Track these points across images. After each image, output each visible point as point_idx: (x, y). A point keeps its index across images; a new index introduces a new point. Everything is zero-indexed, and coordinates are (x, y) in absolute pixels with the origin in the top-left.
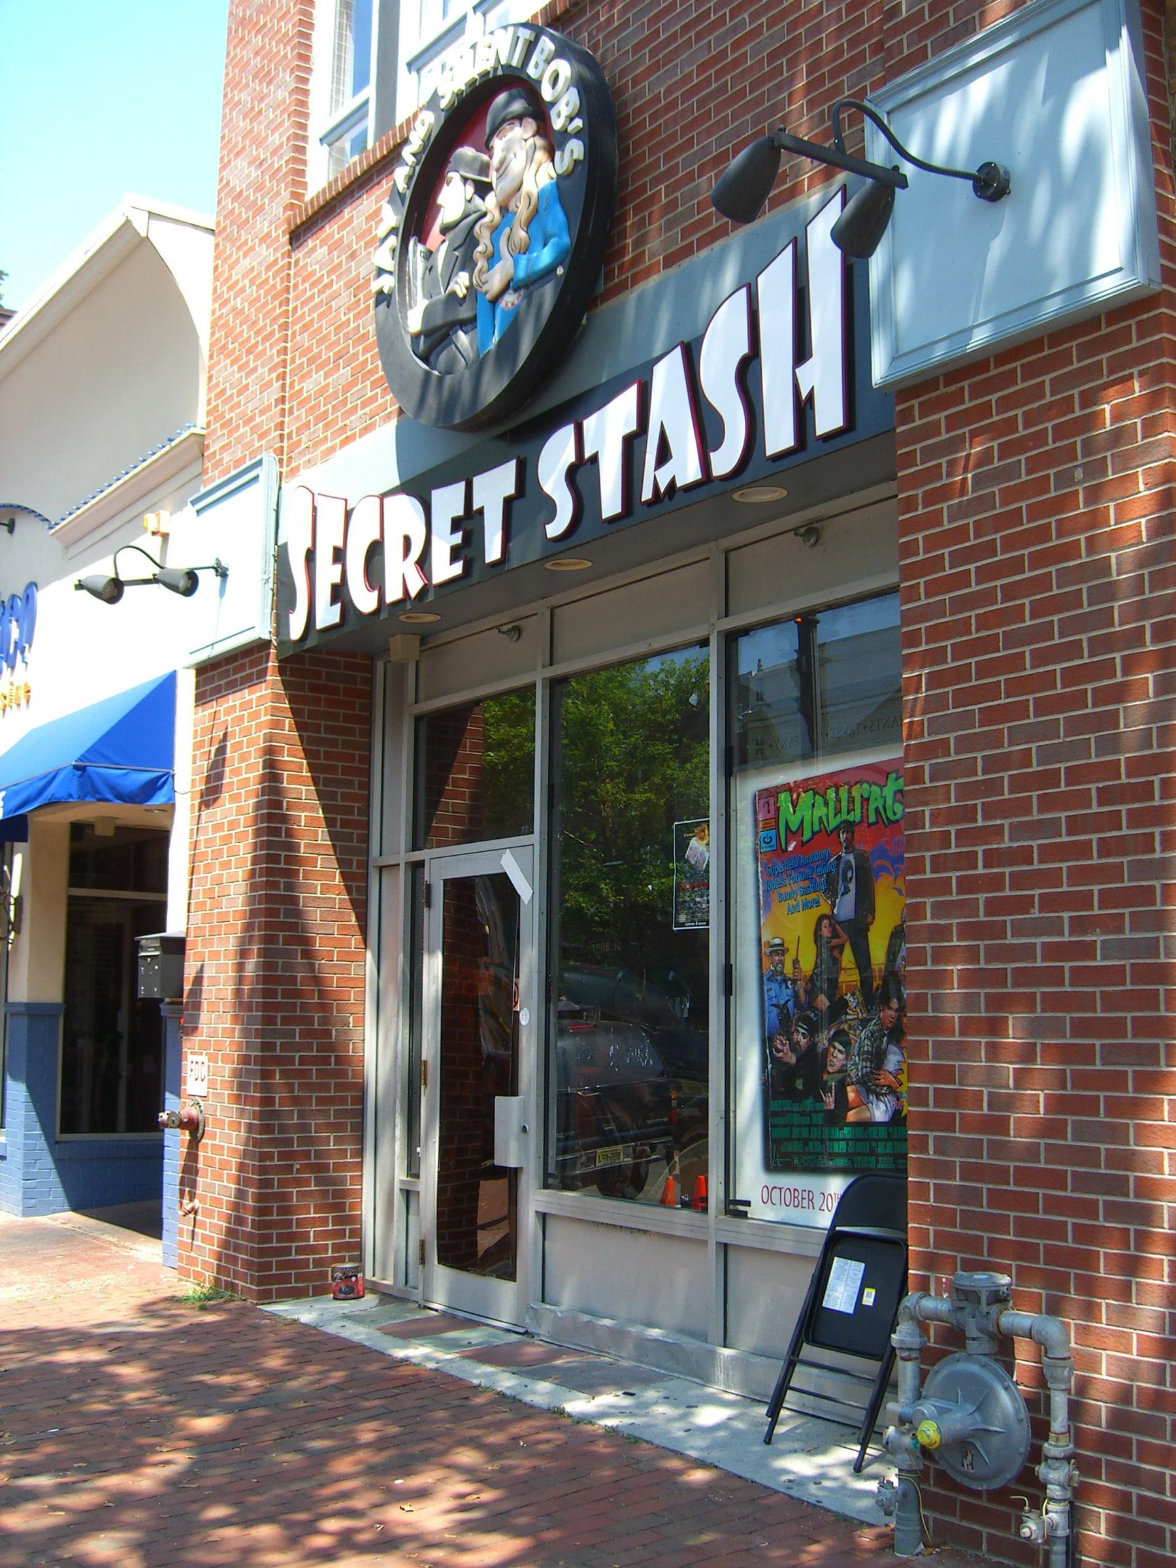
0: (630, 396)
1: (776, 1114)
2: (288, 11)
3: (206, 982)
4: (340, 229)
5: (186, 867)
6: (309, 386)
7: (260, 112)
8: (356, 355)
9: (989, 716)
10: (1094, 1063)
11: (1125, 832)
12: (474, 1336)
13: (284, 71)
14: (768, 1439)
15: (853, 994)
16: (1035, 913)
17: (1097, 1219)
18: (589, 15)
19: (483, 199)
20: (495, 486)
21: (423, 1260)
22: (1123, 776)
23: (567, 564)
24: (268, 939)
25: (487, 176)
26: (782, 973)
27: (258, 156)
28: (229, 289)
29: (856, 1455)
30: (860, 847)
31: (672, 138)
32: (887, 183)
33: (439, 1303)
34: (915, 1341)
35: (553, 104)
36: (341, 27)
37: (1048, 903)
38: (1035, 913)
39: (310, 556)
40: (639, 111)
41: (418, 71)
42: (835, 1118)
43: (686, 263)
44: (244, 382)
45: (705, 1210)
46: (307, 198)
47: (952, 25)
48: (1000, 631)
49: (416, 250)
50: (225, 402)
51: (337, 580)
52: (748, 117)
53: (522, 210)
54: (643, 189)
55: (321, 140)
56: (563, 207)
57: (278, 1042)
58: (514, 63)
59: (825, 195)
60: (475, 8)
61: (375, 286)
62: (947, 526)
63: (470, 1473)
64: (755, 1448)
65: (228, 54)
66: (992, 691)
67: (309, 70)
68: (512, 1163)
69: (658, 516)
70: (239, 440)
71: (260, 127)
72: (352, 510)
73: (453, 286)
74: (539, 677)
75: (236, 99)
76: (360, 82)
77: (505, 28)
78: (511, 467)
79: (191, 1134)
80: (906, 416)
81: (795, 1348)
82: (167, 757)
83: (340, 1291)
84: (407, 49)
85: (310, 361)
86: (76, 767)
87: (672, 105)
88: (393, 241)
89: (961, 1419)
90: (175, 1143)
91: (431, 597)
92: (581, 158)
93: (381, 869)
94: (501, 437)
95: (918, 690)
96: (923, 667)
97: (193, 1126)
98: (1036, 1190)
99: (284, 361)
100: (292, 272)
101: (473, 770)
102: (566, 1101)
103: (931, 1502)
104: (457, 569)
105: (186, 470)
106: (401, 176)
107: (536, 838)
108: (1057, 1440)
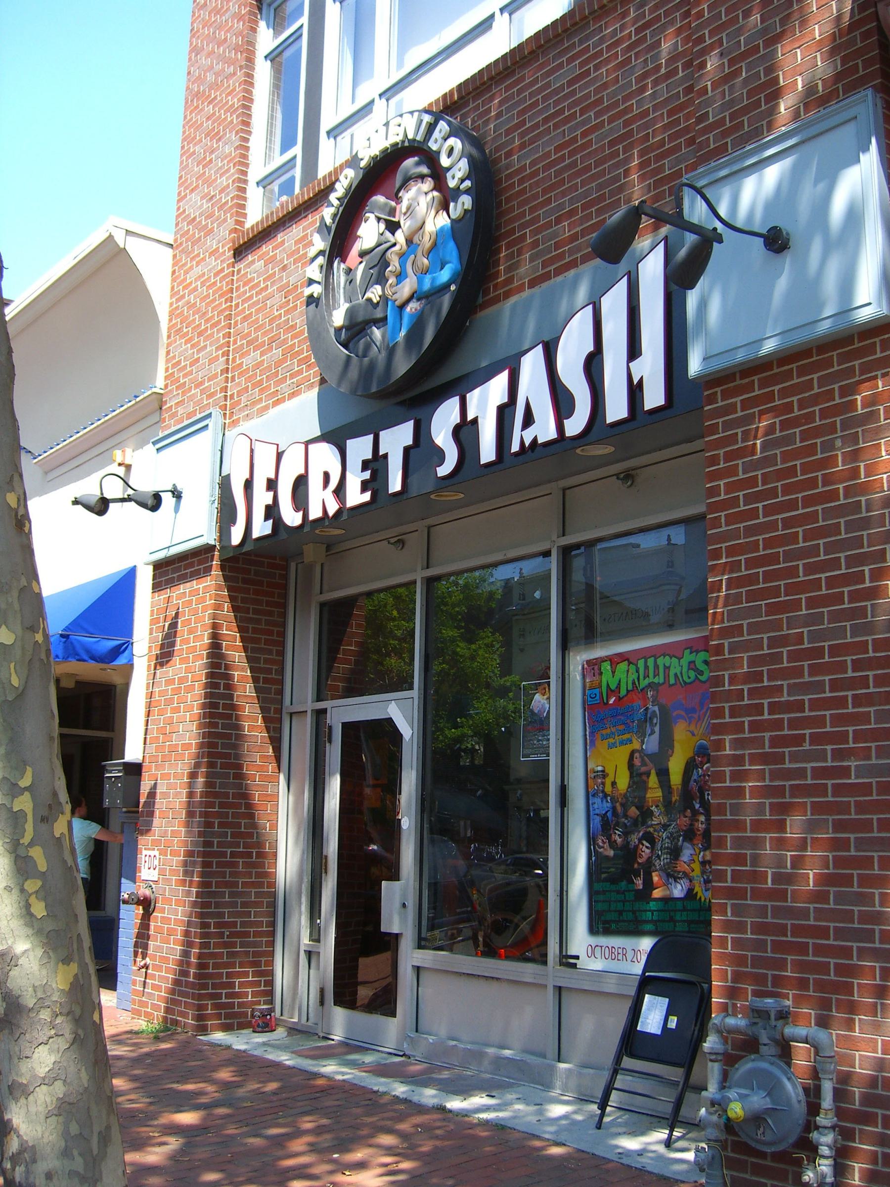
0: (502, 379)
1: (597, 893)
2: (234, 90)
3: (158, 796)
4: (274, 249)
5: (142, 711)
6: (248, 361)
7: (211, 161)
8: (285, 340)
9: (773, 609)
10: (849, 851)
11: (871, 690)
12: (369, 1059)
13: (231, 132)
14: (599, 1126)
15: (657, 806)
16: (807, 746)
17: (852, 959)
18: (471, 106)
19: (393, 234)
20: (397, 439)
21: (322, 1002)
22: (871, 651)
23: (446, 496)
24: (211, 765)
25: (394, 217)
26: (603, 791)
27: (209, 193)
28: (185, 288)
29: (666, 1136)
30: (663, 701)
31: (535, 197)
32: (707, 241)
33: (338, 1036)
34: (720, 1048)
35: (448, 169)
36: (273, 103)
37: (816, 739)
38: (807, 746)
39: (248, 485)
40: (509, 176)
41: (335, 138)
42: (645, 894)
43: (545, 285)
44: (196, 357)
45: (545, 963)
46: (248, 225)
47: (746, 129)
48: (781, 550)
49: (339, 268)
50: (180, 370)
51: (270, 502)
52: (594, 184)
53: (427, 242)
54: (513, 231)
55: (257, 183)
56: (456, 244)
57: (216, 841)
58: (418, 138)
59: (653, 242)
60: (381, 95)
61: (307, 291)
62: (741, 476)
63: (389, 1150)
64: (590, 1132)
65: (185, 117)
66: (776, 592)
67: (249, 133)
68: (395, 930)
69: (525, 465)
70: (191, 398)
71: (210, 172)
72: (284, 451)
73: (369, 295)
74: (419, 576)
75: (192, 150)
76: (287, 143)
77: (412, 113)
78: (409, 426)
79: (144, 909)
80: (711, 399)
81: (618, 1060)
82: (128, 630)
83: (258, 1026)
84: (327, 121)
85: (249, 343)
86: (62, 636)
87: (535, 173)
88: (321, 260)
89: (759, 1101)
90: (129, 919)
91: (345, 516)
92: (470, 208)
93: (291, 714)
94: (401, 403)
95: (719, 590)
96: (723, 574)
97: (147, 904)
98: (807, 940)
99: (229, 342)
100: (235, 278)
101: (358, 644)
102: (434, 887)
103: (731, 1164)
104: (367, 497)
105: (150, 419)
106: (328, 213)
107: (415, 693)
108: (826, 1114)
